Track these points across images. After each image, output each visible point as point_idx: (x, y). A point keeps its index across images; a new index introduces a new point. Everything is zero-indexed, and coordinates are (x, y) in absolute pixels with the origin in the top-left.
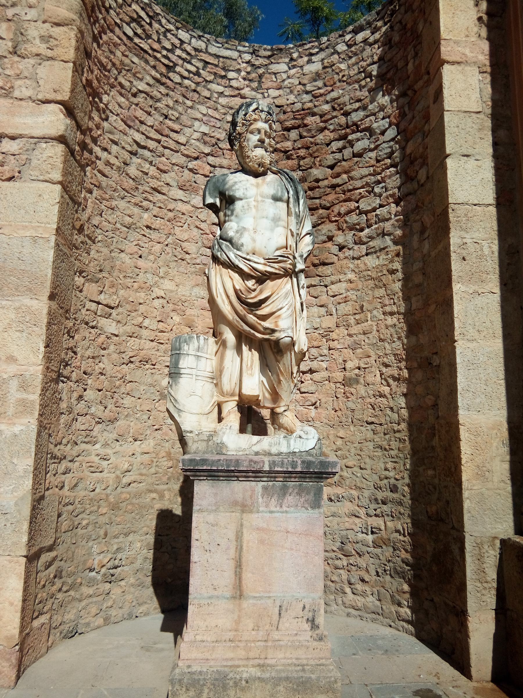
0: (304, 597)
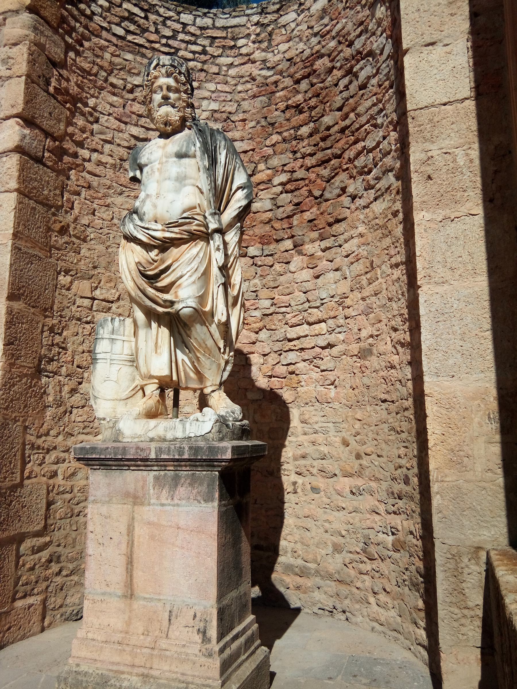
0: (195, 604)
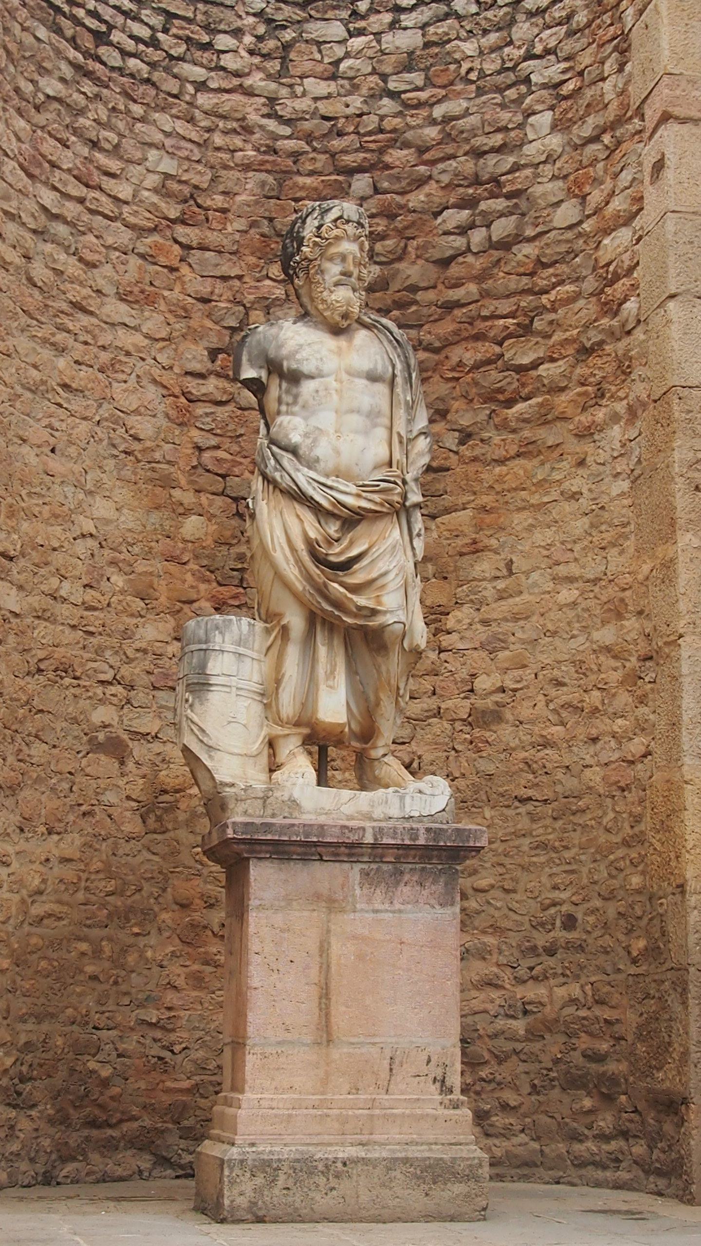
0: (429, 1044)
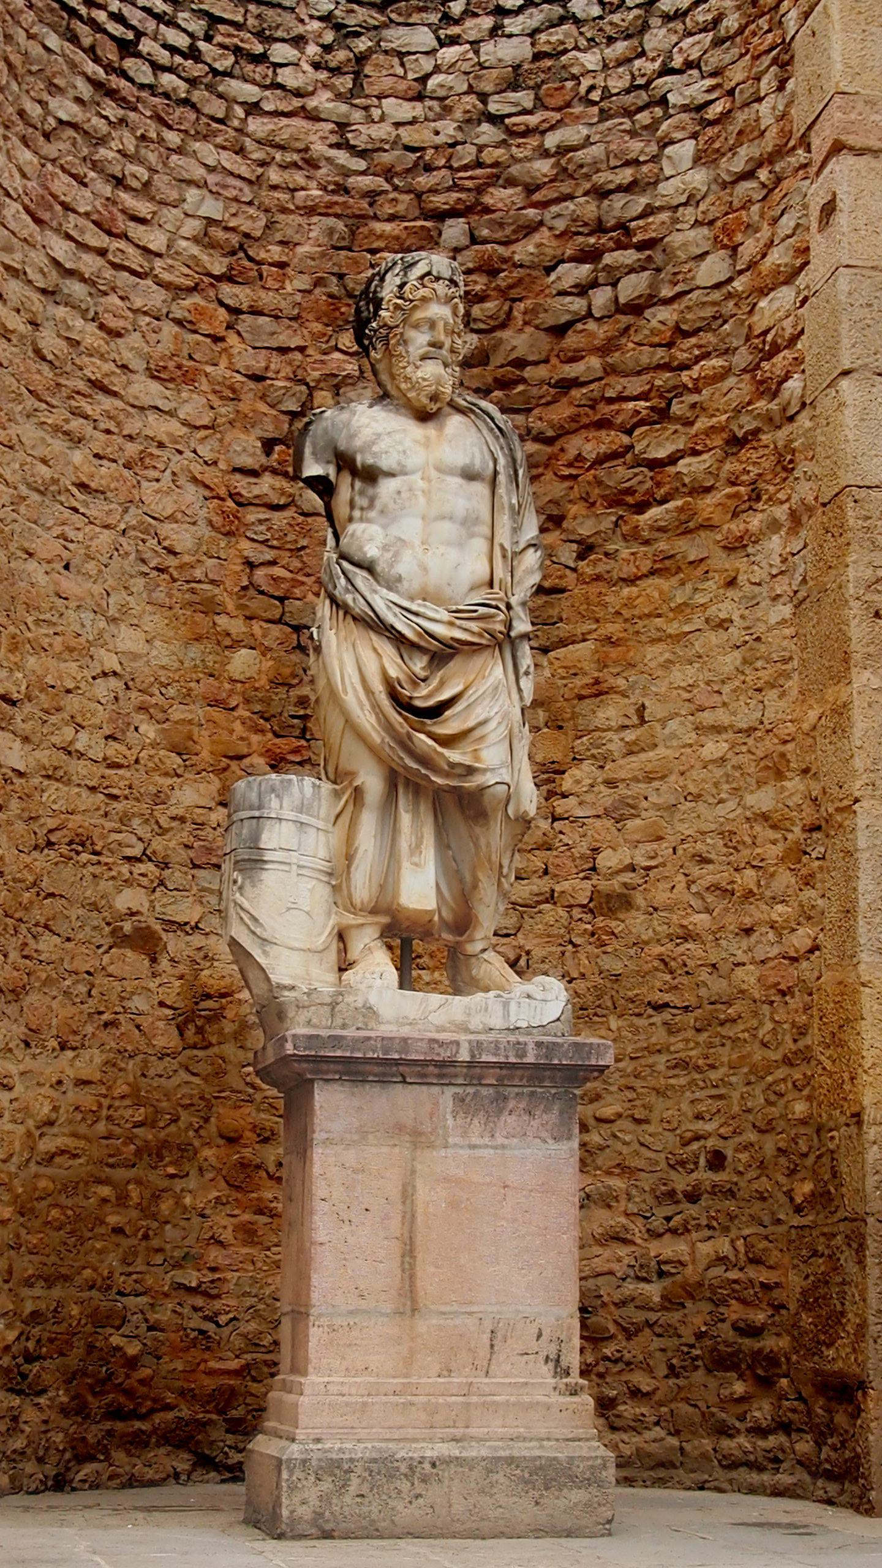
0: (540, 1314)
